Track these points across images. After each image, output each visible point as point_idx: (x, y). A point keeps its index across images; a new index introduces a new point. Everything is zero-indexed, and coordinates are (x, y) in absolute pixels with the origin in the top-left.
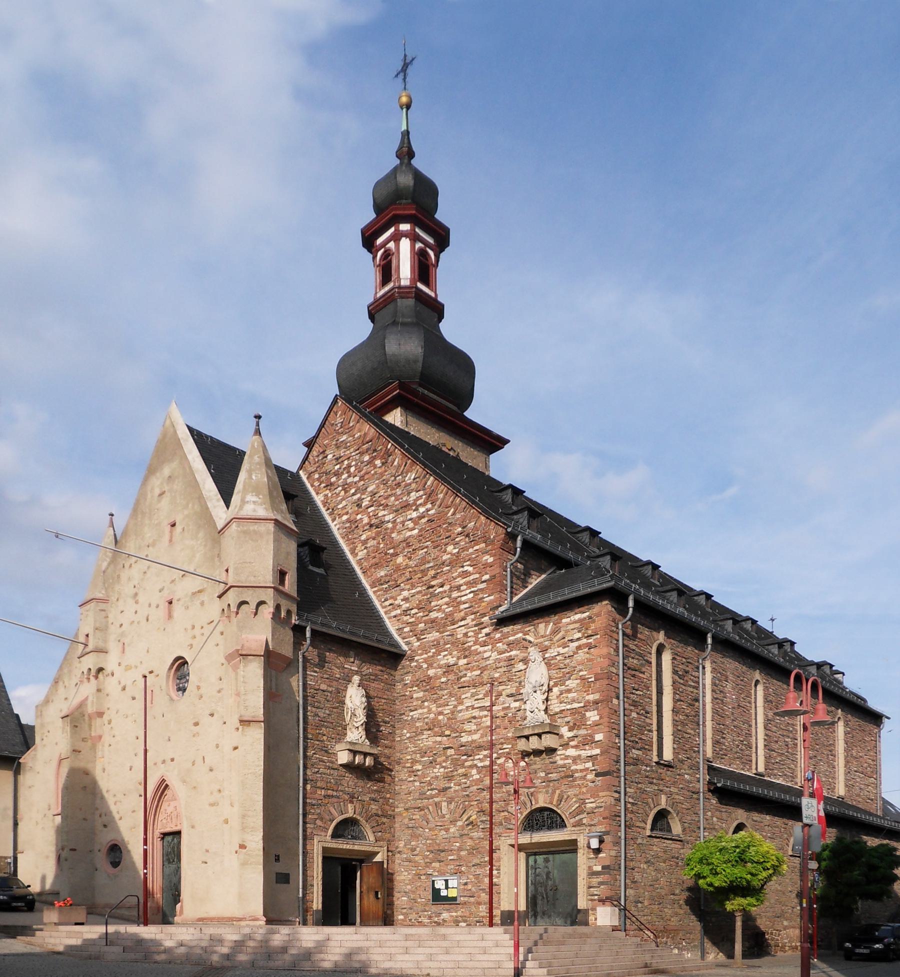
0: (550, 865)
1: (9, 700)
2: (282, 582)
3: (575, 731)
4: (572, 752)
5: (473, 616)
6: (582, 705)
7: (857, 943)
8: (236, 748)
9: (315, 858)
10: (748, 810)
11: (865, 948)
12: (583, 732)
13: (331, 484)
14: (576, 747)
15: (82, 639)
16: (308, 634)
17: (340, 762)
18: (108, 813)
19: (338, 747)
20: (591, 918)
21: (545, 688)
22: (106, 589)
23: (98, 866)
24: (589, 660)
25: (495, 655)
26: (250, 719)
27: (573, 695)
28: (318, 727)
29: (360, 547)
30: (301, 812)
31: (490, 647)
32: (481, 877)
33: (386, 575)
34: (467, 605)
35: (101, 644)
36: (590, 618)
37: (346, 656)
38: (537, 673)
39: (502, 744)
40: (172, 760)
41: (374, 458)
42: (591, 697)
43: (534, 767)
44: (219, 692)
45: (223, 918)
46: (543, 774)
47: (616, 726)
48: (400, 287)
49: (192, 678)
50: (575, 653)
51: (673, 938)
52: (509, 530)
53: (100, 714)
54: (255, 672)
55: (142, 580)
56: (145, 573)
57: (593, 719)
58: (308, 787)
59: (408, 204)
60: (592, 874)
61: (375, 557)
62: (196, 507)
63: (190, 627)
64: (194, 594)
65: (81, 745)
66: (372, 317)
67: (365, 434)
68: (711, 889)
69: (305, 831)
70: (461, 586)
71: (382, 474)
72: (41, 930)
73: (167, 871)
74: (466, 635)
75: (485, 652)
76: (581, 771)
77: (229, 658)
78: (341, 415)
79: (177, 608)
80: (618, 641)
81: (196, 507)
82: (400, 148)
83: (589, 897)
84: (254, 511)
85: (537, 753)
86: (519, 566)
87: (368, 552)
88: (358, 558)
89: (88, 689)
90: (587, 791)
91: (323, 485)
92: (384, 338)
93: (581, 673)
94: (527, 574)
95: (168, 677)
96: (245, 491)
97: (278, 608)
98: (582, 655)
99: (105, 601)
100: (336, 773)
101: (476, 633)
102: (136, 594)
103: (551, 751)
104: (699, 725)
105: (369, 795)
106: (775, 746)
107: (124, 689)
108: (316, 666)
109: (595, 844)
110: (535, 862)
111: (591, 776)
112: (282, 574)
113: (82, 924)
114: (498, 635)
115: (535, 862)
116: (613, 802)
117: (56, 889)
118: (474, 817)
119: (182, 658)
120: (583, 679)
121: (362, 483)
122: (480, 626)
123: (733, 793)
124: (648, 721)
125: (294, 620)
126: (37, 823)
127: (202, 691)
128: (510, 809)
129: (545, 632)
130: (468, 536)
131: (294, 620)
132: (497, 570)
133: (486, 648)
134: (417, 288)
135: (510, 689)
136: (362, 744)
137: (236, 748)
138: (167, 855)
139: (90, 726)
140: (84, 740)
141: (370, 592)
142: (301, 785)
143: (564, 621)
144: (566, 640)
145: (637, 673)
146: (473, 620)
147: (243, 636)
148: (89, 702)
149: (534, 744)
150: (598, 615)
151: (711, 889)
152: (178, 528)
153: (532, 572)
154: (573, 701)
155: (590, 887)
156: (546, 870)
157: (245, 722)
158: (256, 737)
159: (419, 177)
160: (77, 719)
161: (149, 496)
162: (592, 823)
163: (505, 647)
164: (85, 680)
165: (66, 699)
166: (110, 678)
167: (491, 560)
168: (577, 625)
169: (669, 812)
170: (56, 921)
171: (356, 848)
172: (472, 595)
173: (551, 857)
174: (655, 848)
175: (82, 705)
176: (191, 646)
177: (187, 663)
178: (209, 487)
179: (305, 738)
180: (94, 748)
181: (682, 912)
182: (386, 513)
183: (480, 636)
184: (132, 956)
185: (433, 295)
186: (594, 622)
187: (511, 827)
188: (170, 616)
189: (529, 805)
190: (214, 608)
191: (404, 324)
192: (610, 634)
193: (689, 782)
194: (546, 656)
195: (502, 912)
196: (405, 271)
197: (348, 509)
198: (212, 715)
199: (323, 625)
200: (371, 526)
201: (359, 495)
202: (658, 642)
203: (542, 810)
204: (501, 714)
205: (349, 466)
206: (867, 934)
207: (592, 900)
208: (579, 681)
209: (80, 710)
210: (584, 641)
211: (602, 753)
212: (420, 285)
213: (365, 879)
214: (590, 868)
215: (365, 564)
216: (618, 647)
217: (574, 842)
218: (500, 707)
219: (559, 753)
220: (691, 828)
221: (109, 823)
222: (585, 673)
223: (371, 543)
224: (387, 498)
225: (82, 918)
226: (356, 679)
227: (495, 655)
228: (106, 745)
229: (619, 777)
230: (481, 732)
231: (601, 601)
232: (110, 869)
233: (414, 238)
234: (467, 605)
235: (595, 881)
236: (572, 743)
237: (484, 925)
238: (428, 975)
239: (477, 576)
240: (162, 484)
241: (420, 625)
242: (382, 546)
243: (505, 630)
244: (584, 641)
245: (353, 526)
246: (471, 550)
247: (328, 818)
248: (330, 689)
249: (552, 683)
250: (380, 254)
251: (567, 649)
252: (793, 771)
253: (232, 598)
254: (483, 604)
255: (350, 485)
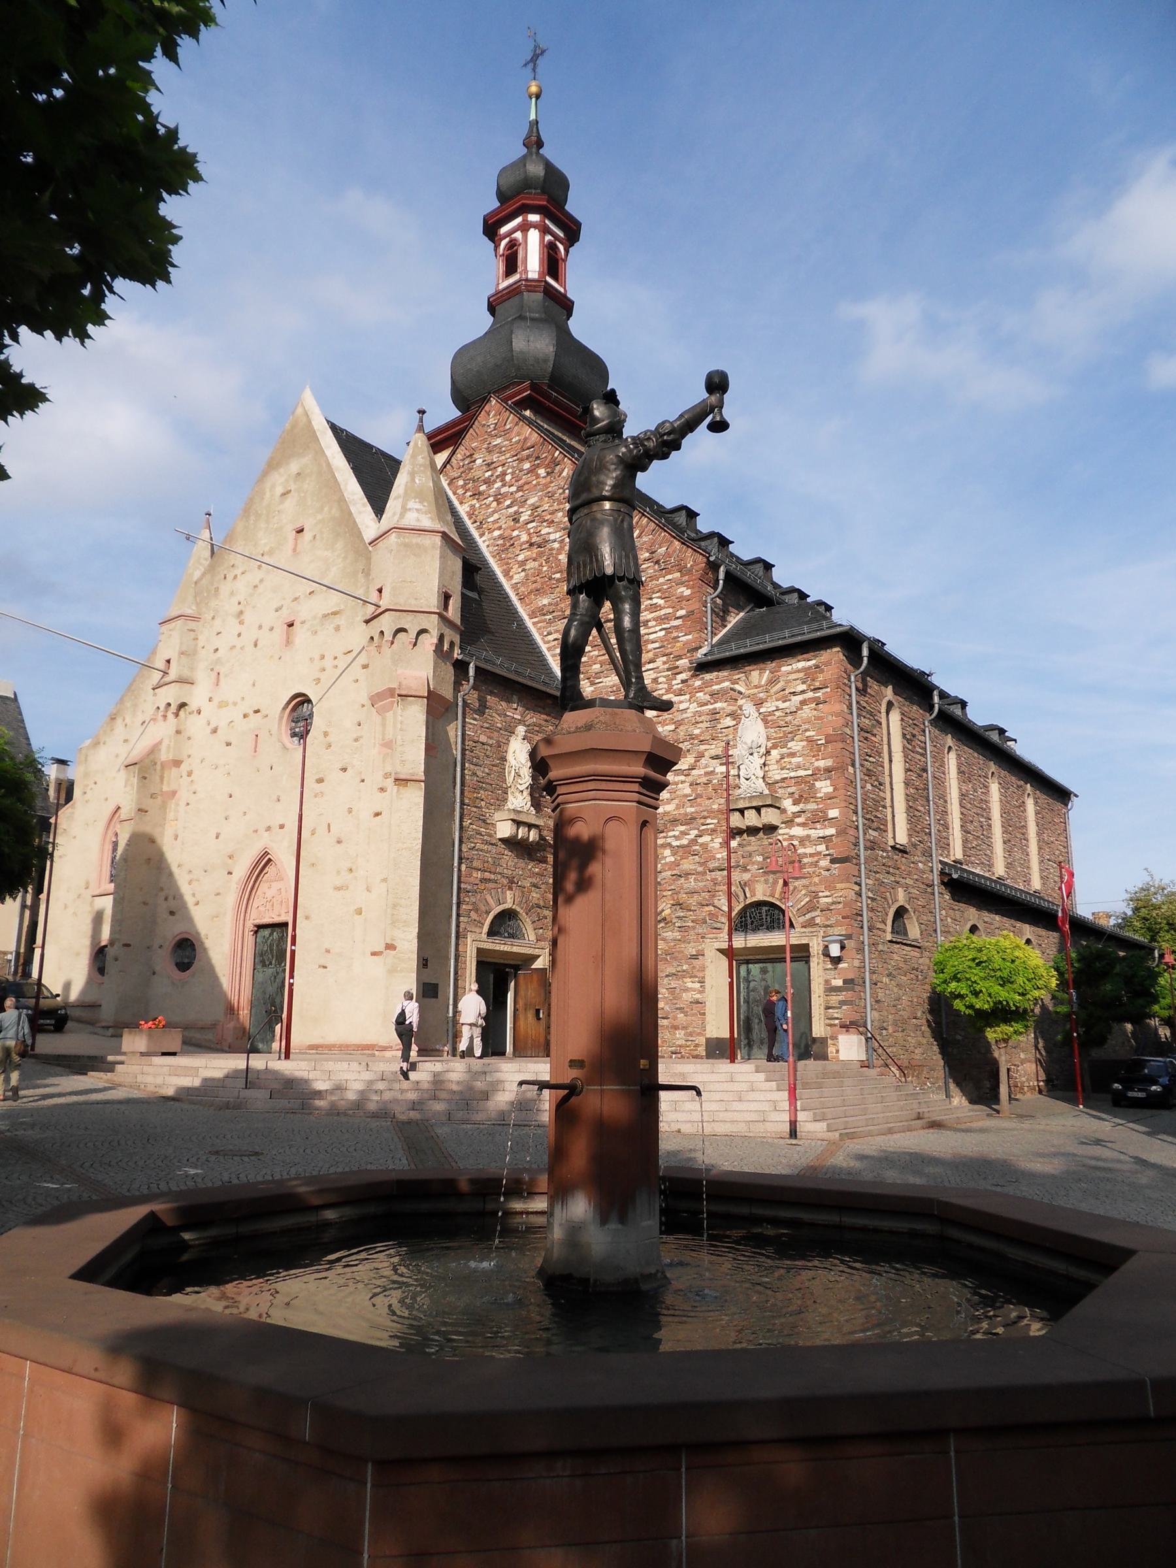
0: (769, 976)
1: (28, 739)
2: (446, 607)
3: (801, 805)
4: (797, 831)
5: (665, 659)
6: (810, 772)
7: (1129, 1084)
8: (377, 814)
9: (468, 963)
10: (979, 908)
11: (1140, 1090)
12: (812, 806)
13: (480, 493)
14: (803, 825)
15: (160, 664)
16: (472, 672)
17: (500, 835)
18: (178, 896)
19: (498, 816)
20: (831, 1050)
21: (763, 750)
22: (198, 605)
23: (157, 969)
24: (817, 718)
25: (693, 707)
26: (409, 777)
27: (799, 760)
28: (476, 789)
29: (515, 568)
30: (455, 901)
31: (687, 697)
32: (678, 991)
33: (550, 604)
34: (657, 645)
35: (186, 673)
36: (817, 667)
37: (509, 701)
38: (752, 731)
39: (705, 818)
40: (282, 827)
41: (538, 466)
42: (822, 764)
43: (748, 848)
44: (356, 740)
45: (347, 1046)
46: (760, 859)
47: (853, 801)
48: (527, 280)
49: (317, 721)
50: (798, 709)
51: (918, 1077)
52: (712, 559)
53: (177, 763)
54: (415, 717)
55: (252, 595)
56: (256, 587)
57: (824, 790)
58: (463, 867)
59: (537, 193)
60: (830, 990)
61: (535, 582)
62: (334, 511)
63: (317, 657)
64: (325, 616)
65: (148, 803)
66: (492, 309)
67: (526, 439)
68: (968, 1011)
69: (458, 926)
70: (648, 621)
71: (546, 486)
72: (122, 1063)
73: (260, 977)
74: (655, 680)
75: (681, 702)
76: (811, 855)
77: (375, 699)
78: (495, 415)
79: (301, 634)
80: (850, 696)
81: (334, 511)
82: (528, 137)
83: (828, 1022)
84: (418, 520)
85: (752, 831)
86: (718, 601)
87: (527, 575)
88: (514, 581)
89: (162, 730)
90: (820, 881)
91: (469, 494)
92: (512, 332)
93: (808, 734)
94: (726, 612)
95: (281, 718)
96: (406, 496)
97: (441, 638)
98: (807, 712)
99: (195, 618)
100: (494, 849)
101: (669, 680)
102: (241, 612)
103: (771, 829)
104: (928, 801)
105: (530, 880)
106: (970, 827)
107: (215, 731)
108: (475, 711)
109: (835, 951)
110: (749, 972)
111: (824, 863)
112: (447, 597)
113: (174, 1054)
114: (698, 683)
115: (749, 972)
116: (854, 897)
117: (90, 999)
118: (667, 912)
119: (304, 695)
120: (809, 740)
121: (521, 494)
122: (675, 670)
123: (966, 889)
124: (881, 794)
125: (457, 654)
126: (66, 907)
127: (330, 739)
128: (716, 902)
129: (760, 680)
130: (657, 562)
131: (457, 654)
132: (695, 605)
133: (682, 698)
134: (546, 282)
135: (716, 749)
136: (527, 813)
137: (377, 814)
138: (261, 955)
139: (162, 778)
140: (153, 796)
141: (529, 623)
142: (456, 864)
143: (783, 669)
144: (787, 692)
145: (868, 735)
146: (664, 663)
147: (399, 672)
148: (164, 747)
149: (751, 819)
150: (828, 664)
151: (968, 1011)
152: (307, 535)
153: (731, 609)
154: (798, 767)
155: (828, 1008)
156: (763, 983)
157: (401, 782)
158: (415, 798)
159: (549, 167)
160: (146, 769)
161: (268, 494)
162: (828, 923)
163: (708, 697)
164: (160, 718)
165: (126, 741)
166: (195, 716)
167: (688, 592)
168: (801, 675)
169: (907, 910)
170: (143, 1049)
171: (515, 949)
172: (663, 633)
173: (769, 966)
174: (895, 957)
175: (154, 750)
176: (318, 680)
177: (309, 701)
178: (352, 488)
179: (462, 803)
180: (164, 807)
181: (924, 1041)
182: (551, 530)
183: (674, 682)
184: (283, 1103)
185: (562, 290)
186: (822, 671)
187: (719, 925)
188: (288, 642)
189: (742, 898)
190: (358, 635)
191: (532, 319)
192: (842, 686)
193: (923, 872)
194: (762, 710)
195: (708, 1040)
196: (533, 264)
197: (502, 523)
198: (344, 770)
199: (486, 661)
200: (531, 545)
201: (515, 508)
202: (887, 699)
203: (759, 904)
204: (704, 780)
205: (504, 474)
206: (1133, 1073)
207: (831, 1025)
208: (805, 743)
209: (152, 757)
210: (810, 695)
211: (839, 834)
212: (548, 279)
213: (522, 993)
214: (827, 982)
215: (523, 589)
216: (851, 705)
217: (805, 948)
218: (702, 772)
219: (781, 831)
220: (929, 930)
221: (177, 909)
222: (813, 733)
223: (530, 565)
224: (552, 513)
225: (175, 1045)
226: (521, 730)
227: (693, 707)
228: (183, 803)
229: (858, 864)
230: (676, 801)
231: (831, 647)
232: (177, 974)
233: (544, 230)
234: (657, 645)
235: (835, 999)
236: (798, 820)
237: (683, 1057)
238: (679, 1131)
239: (670, 610)
240: (287, 481)
241: (594, 667)
242: (545, 569)
243: (708, 676)
244: (810, 695)
245: (507, 544)
246: (661, 580)
247: (483, 908)
248: (490, 742)
249: (770, 744)
250: (504, 243)
251: (787, 704)
252: (990, 858)
253: (387, 623)
254: (678, 644)
255: (505, 496)
